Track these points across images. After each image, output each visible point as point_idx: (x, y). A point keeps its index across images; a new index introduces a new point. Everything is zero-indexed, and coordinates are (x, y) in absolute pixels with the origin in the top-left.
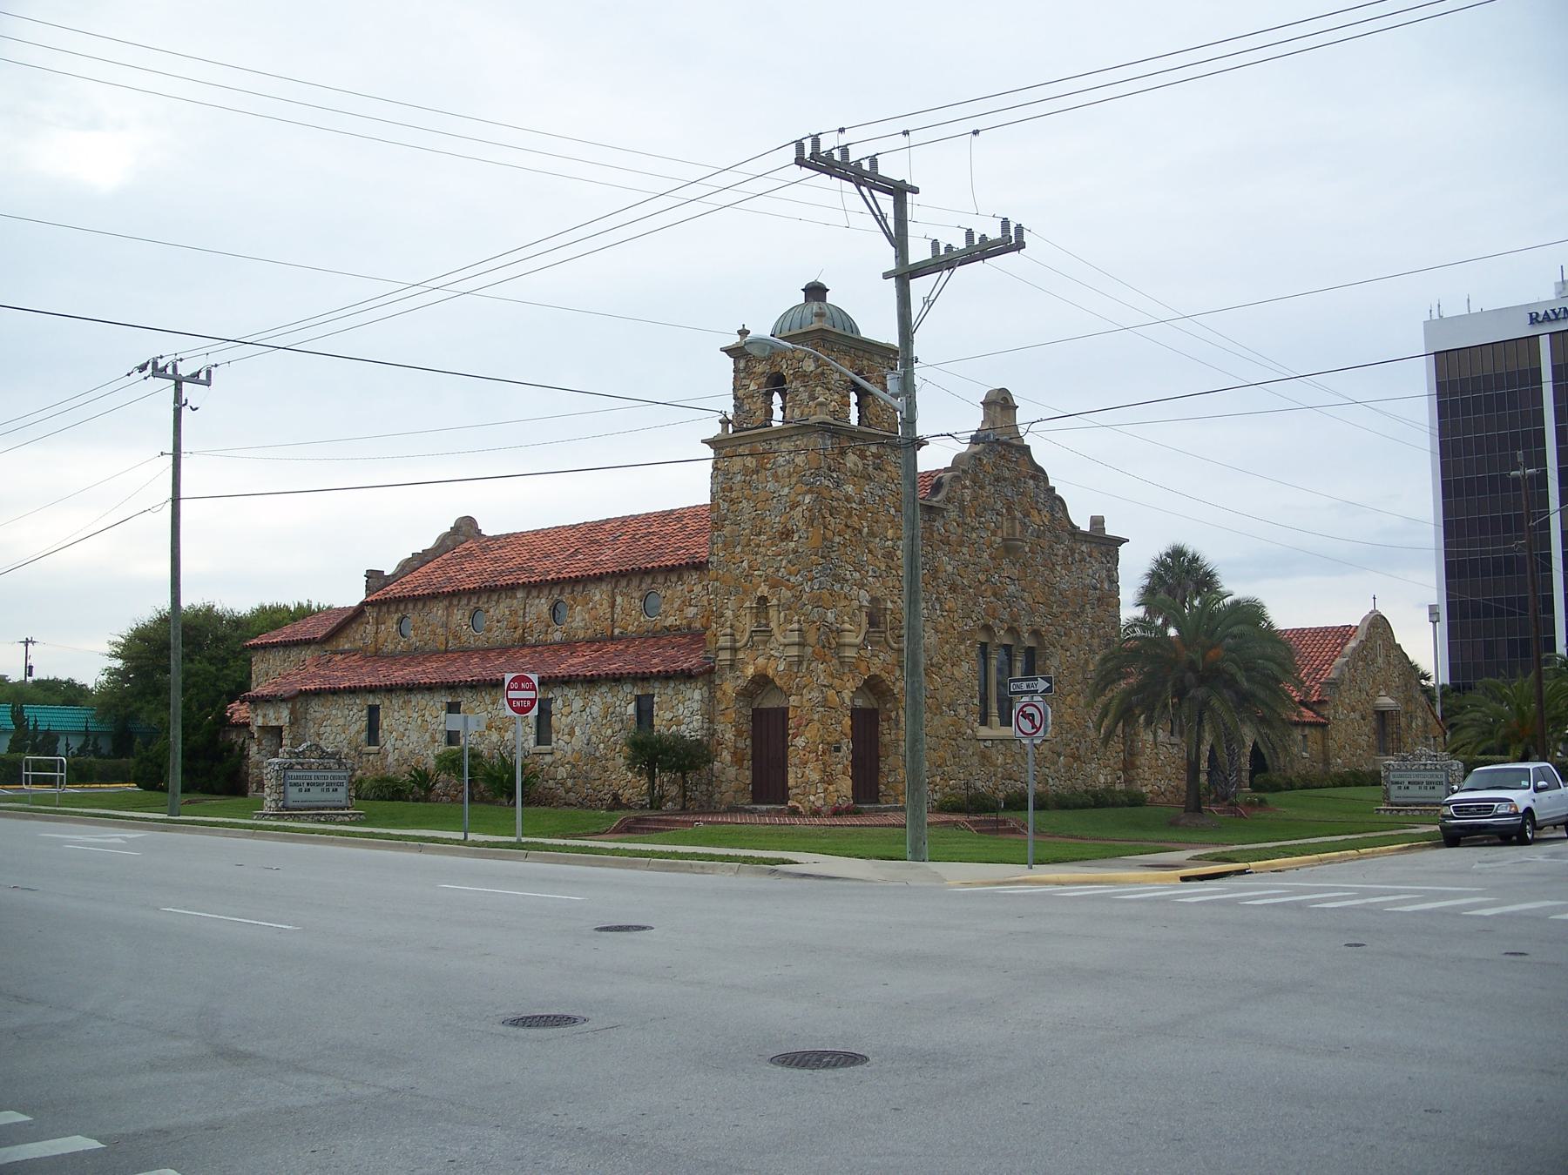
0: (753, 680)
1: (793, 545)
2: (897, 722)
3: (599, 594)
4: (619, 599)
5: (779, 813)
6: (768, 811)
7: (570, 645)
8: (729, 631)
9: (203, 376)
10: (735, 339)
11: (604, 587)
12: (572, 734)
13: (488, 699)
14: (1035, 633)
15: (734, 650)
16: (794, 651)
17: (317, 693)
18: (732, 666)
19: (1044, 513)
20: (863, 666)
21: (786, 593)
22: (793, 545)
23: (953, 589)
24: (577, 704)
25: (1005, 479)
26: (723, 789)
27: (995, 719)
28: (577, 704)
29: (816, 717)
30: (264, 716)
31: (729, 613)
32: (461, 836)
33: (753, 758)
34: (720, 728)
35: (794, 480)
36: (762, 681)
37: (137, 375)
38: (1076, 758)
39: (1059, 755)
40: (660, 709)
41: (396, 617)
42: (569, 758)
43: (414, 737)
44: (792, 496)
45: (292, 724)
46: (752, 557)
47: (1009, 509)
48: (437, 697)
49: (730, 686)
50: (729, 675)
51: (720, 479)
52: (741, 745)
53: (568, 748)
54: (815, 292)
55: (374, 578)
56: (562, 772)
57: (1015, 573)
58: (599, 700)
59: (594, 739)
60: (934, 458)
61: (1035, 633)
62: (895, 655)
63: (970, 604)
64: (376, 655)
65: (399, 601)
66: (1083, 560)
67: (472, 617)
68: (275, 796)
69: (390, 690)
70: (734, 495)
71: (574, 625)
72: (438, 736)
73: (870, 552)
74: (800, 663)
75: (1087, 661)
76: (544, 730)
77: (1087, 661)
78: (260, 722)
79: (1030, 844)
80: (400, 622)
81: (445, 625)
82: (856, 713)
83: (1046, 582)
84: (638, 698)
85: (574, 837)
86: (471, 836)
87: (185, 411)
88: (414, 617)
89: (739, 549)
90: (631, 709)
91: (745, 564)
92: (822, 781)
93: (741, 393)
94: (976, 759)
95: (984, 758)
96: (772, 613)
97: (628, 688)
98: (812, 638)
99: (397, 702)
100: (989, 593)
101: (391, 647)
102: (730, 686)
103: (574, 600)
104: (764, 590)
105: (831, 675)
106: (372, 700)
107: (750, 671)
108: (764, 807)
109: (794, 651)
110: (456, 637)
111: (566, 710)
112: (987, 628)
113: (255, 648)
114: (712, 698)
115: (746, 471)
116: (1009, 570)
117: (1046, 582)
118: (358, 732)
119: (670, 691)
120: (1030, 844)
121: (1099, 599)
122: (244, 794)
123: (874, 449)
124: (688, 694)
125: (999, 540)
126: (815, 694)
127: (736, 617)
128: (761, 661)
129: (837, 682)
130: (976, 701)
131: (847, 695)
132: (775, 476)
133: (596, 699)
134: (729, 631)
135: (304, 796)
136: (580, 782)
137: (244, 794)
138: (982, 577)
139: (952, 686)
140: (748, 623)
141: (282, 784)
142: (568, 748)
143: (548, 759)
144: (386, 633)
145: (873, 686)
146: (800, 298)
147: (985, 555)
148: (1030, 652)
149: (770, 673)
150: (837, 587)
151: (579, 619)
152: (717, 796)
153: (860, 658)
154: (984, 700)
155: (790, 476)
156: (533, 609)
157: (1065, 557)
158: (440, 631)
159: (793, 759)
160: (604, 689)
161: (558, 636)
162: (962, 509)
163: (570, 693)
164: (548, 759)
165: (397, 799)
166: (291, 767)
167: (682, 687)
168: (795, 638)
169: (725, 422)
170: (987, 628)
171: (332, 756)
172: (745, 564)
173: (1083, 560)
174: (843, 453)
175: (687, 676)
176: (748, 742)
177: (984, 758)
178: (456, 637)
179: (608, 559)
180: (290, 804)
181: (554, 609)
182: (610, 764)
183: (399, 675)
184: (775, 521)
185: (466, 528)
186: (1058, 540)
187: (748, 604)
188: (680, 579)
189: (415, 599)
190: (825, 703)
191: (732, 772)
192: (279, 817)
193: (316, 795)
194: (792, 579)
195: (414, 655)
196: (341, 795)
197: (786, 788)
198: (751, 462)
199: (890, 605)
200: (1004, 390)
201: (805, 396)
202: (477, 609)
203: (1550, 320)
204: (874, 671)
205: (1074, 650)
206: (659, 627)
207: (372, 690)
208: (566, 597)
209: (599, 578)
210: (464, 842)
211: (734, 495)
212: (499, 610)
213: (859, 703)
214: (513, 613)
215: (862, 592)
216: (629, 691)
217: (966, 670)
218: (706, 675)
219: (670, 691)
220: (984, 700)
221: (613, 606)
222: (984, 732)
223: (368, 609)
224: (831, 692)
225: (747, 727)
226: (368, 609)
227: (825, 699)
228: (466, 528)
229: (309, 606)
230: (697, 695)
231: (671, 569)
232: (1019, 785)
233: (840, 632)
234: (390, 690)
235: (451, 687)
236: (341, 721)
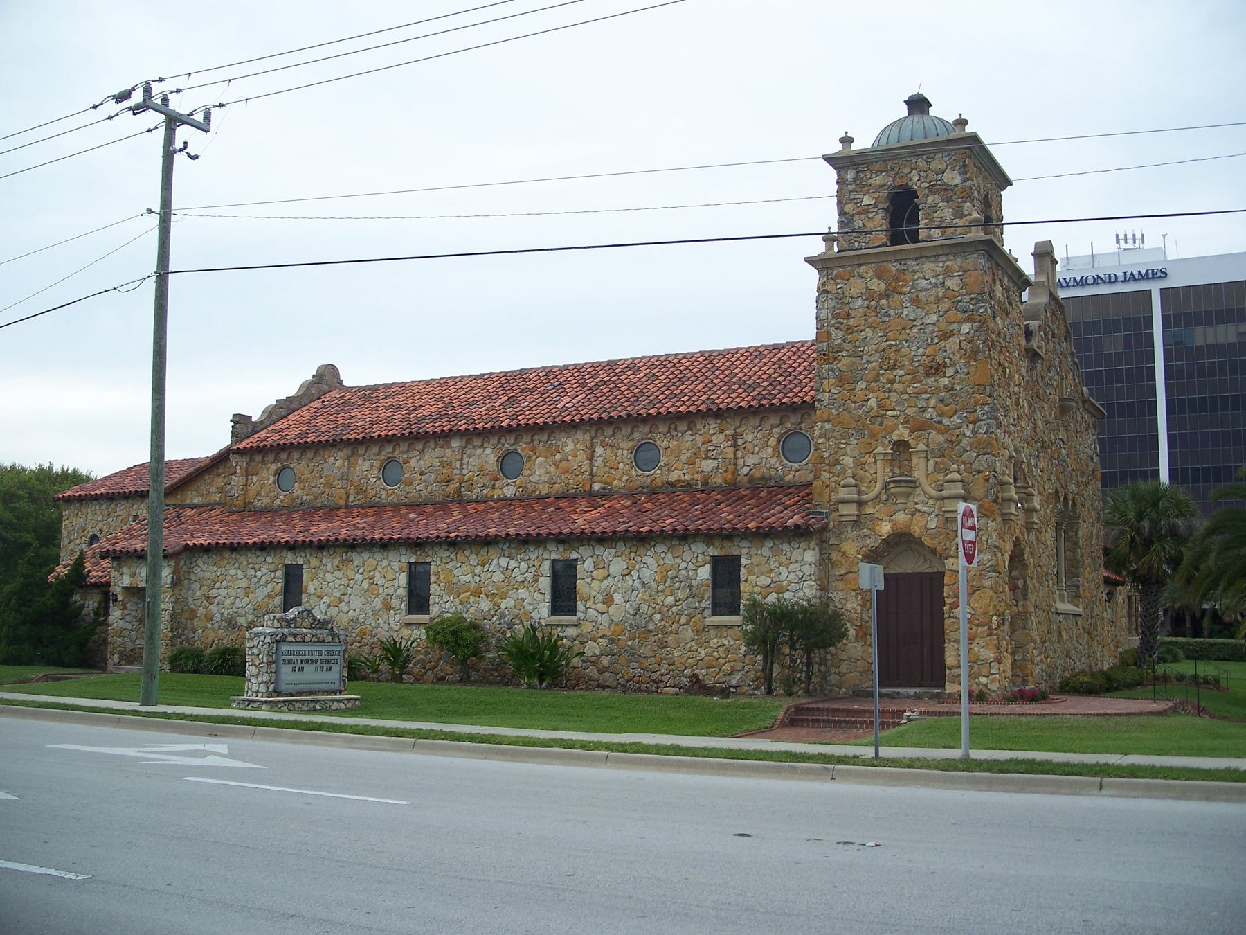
1: (945, 381)
3: (570, 445)
4: (599, 451)
5: (934, 697)
6: (917, 697)
7: (527, 500)
9: (199, 117)
10: (836, 148)
11: (579, 435)
12: (608, 601)
13: (474, 559)
15: (860, 504)
17: (207, 550)
18: (857, 524)
21: (936, 438)
22: (945, 381)
24: (618, 566)
26: (843, 668)
30: (133, 575)
31: (847, 461)
32: (869, 752)
35: (945, 306)
36: (901, 541)
37: (112, 107)
40: (750, 573)
41: (273, 467)
42: (604, 629)
43: (357, 603)
44: (943, 324)
46: (882, 395)
48: (393, 556)
50: (851, 533)
51: (832, 303)
53: (604, 620)
54: (918, 104)
55: (240, 421)
56: (592, 648)
58: (651, 563)
59: (644, 608)
64: (247, 510)
65: (279, 449)
67: (384, 468)
68: (266, 678)
69: (321, 547)
70: (852, 322)
71: (534, 479)
72: (395, 603)
76: (564, 596)
78: (127, 581)
79: (965, 720)
80: (278, 473)
84: (715, 561)
85: (1200, 752)
86: (885, 752)
87: (179, 159)
88: (300, 466)
89: (862, 385)
90: (705, 572)
91: (873, 403)
93: (849, 208)
97: (699, 548)
99: (330, 561)
101: (266, 501)
103: (534, 450)
104: (902, 433)
106: (290, 558)
108: (912, 691)
111: (599, 574)
113: (68, 500)
118: (269, 597)
119: (766, 551)
120: (965, 720)
122: (104, 669)
124: (796, 555)
127: (860, 464)
128: (901, 517)
132: (916, 302)
133: (649, 560)
134: (852, 481)
135: (298, 677)
136: (622, 660)
137: (104, 669)
140: (880, 472)
141: (275, 660)
142: (604, 620)
143: (571, 632)
144: (262, 484)
146: (903, 111)
149: (916, 530)
151: (540, 472)
152: (833, 678)
155: (938, 301)
156: (474, 461)
160: (660, 548)
161: (510, 491)
163: (607, 553)
164: (571, 632)
165: (380, 681)
166: (283, 640)
167: (785, 547)
169: (828, 238)
171: (324, 624)
172: (873, 403)
175: (799, 534)
178: (359, 490)
179: (570, 403)
180: (284, 687)
181: (502, 461)
182: (670, 638)
183: (321, 530)
184: (918, 353)
185: (327, 377)
187: (880, 449)
188: (689, 428)
189: (304, 447)
192: (273, 705)
193: (310, 675)
194: (945, 421)
195: (307, 511)
196: (335, 675)
197: (943, 667)
198: (878, 285)
201: (948, 213)
202: (391, 460)
203: (1135, 279)
206: (659, 481)
207: (292, 547)
208: (522, 447)
209: (574, 426)
210: (877, 761)
211: (852, 322)
216: (542, 561)
223: (234, 459)
226: (234, 459)
228: (327, 377)
229: (51, 469)
231: (679, 417)
234: (321, 547)
235: (417, 545)
236: (244, 583)
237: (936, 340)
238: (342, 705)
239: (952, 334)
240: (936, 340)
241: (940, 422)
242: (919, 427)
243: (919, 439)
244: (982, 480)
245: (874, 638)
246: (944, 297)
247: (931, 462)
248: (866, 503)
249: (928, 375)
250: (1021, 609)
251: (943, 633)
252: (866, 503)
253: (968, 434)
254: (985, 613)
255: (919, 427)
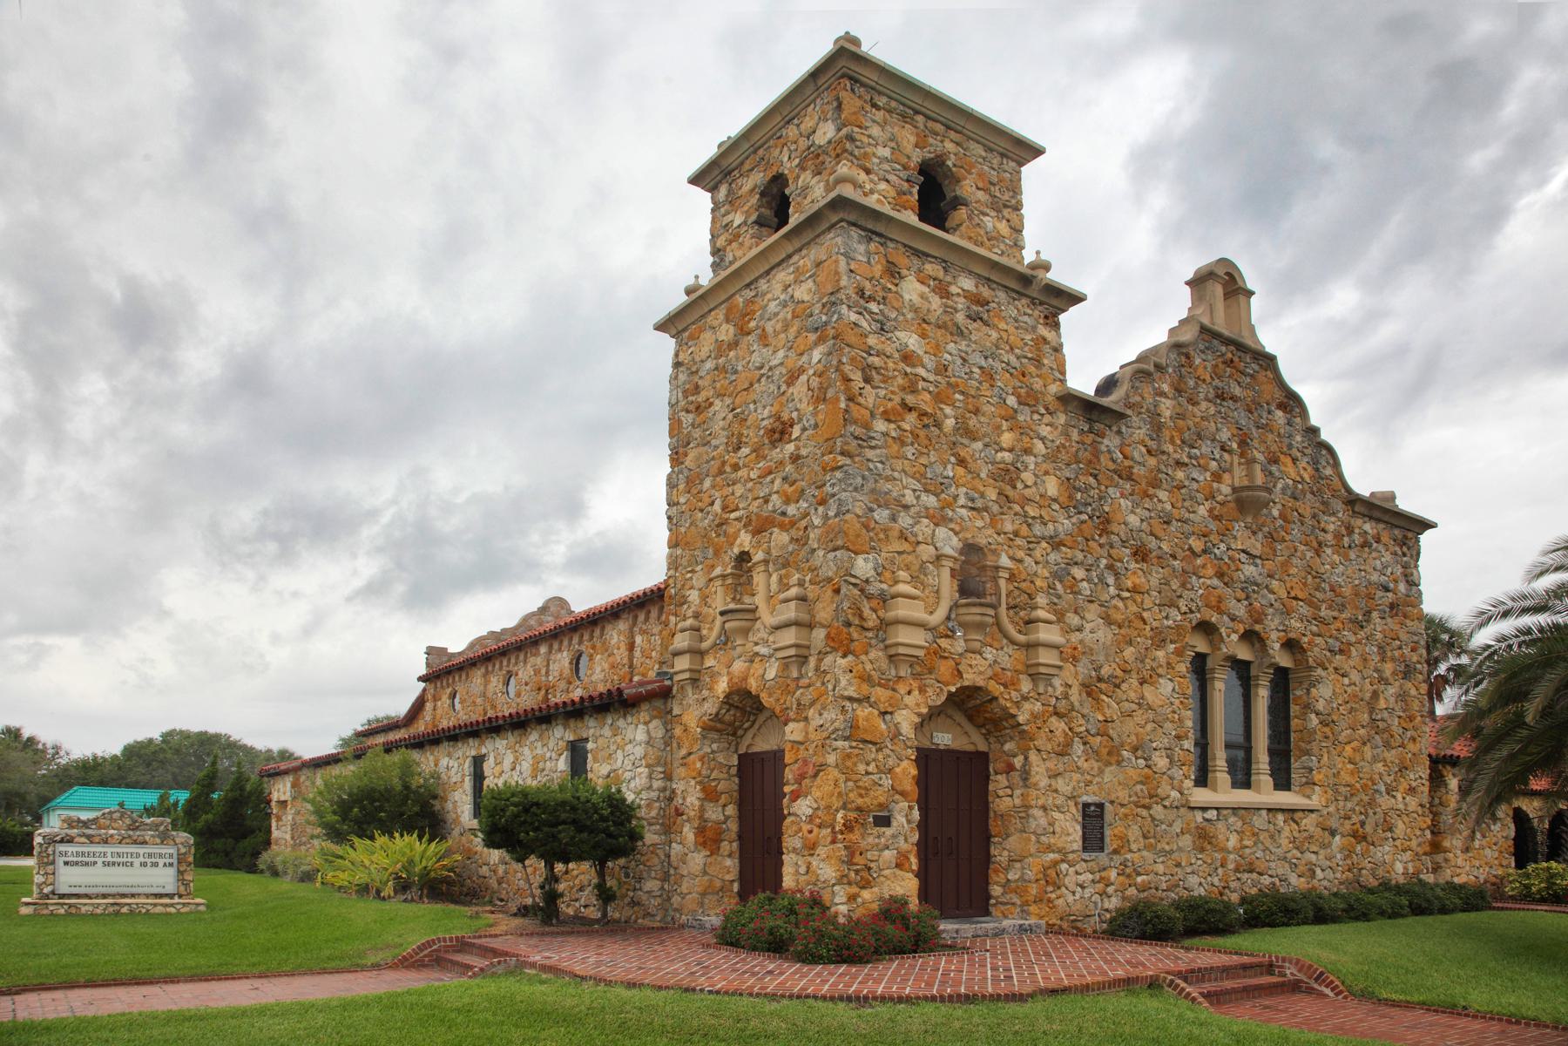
0: (728, 700)
2: (1026, 775)
4: (638, 639)
8: (689, 622)
14: (1290, 645)
16: (789, 637)
18: (695, 681)
19: (1303, 463)
20: (944, 668)
21: (780, 538)
22: (790, 448)
23: (1141, 554)
25: (1234, 398)
26: (684, 889)
27: (1222, 777)
28: (509, 759)
29: (831, 759)
31: (694, 596)
33: (740, 837)
34: (679, 786)
38: (1358, 836)
39: (1333, 833)
40: (595, 760)
45: (294, 798)
47: (1243, 443)
49: (694, 711)
50: (691, 695)
51: (682, 378)
52: (714, 814)
57: (1256, 546)
60: (1091, 354)
61: (1290, 645)
62: (1020, 655)
63: (1175, 584)
66: (1365, 544)
71: (594, 678)
73: (962, 462)
74: (803, 660)
75: (1375, 694)
77: (1375, 694)
81: (484, 695)
82: (927, 759)
83: (1309, 569)
89: (707, 483)
91: (717, 507)
92: (842, 879)
94: (1187, 841)
95: (1204, 838)
96: (759, 578)
98: (824, 612)
100: (1210, 571)
102: (694, 711)
103: (594, 647)
104: (745, 540)
105: (865, 678)
107: (722, 686)
109: (789, 637)
110: (494, 707)
112: (1206, 628)
114: (668, 739)
115: (721, 349)
116: (1242, 537)
117: (1309, 569)
119: (607, 731)
121: (1392, 606)
123: (967, 283)
125: (1226, 489)
126: (830, 715)
128: (739, 666)
129: (880, 693)
130: (1188, 744)
131: (906, 721)
132: (764, 339)
133: (526, 751)
138: (1197, 545)
139: (1139, 717)
145: (968, 704)
147: (1202, 510)
148: (1282, 680)
149: (753, 685)
150: (881, 515)
152: (676, 900)
153: (939, 653)
154: (1203, 745)
155: (786, 328)
157: (1338, 536)
158: (479, 701)
159: (791, 841)
162: (1157, 427)
167: (621, 723)
168: (790, 612)
170: (1206, 628)
173: (1365, 544)
174: (893, 272)
176: (731, 810)
177: (1204, 838)
186: (1327, 509)
187: (718, 571)
190: (853, 731)
191: (697, 859)
194: (791, 510)
199: (1004, 561)
200: (1224, 262)
204: (970, 678)
205: (1355, 676)
212: (526, 669)
213: (944, 739)
214: (537, 672)
215: (942, 532)
216: (560, 734)
217: (1169, 690)
218: (658, 697)
219: (607, 731)
220: (1203, 745)
221: (631, 647)
222: (1201, 796)
224: (863, 712)
225: (728, 784)
227: (854, 725)
230: (640, 734)
232: (1266, 880)
233: (884, 599)
237: (784, 388)
238: (172, 910)
239: (802, 370)
240: (784, 388)
241: (784, 514)
242: (760, 527)
243: (758, 545)
244: (829, 592)
245: (729, 846)
246: (794, 317)
247: (775, 578)
248: (707, 652)
249: (773, 444)
250: (1017, 801)
251: (780, 841)
252: (707, 652)
253: (817, 521)
254: (828, 807)
255: (760, 527)
